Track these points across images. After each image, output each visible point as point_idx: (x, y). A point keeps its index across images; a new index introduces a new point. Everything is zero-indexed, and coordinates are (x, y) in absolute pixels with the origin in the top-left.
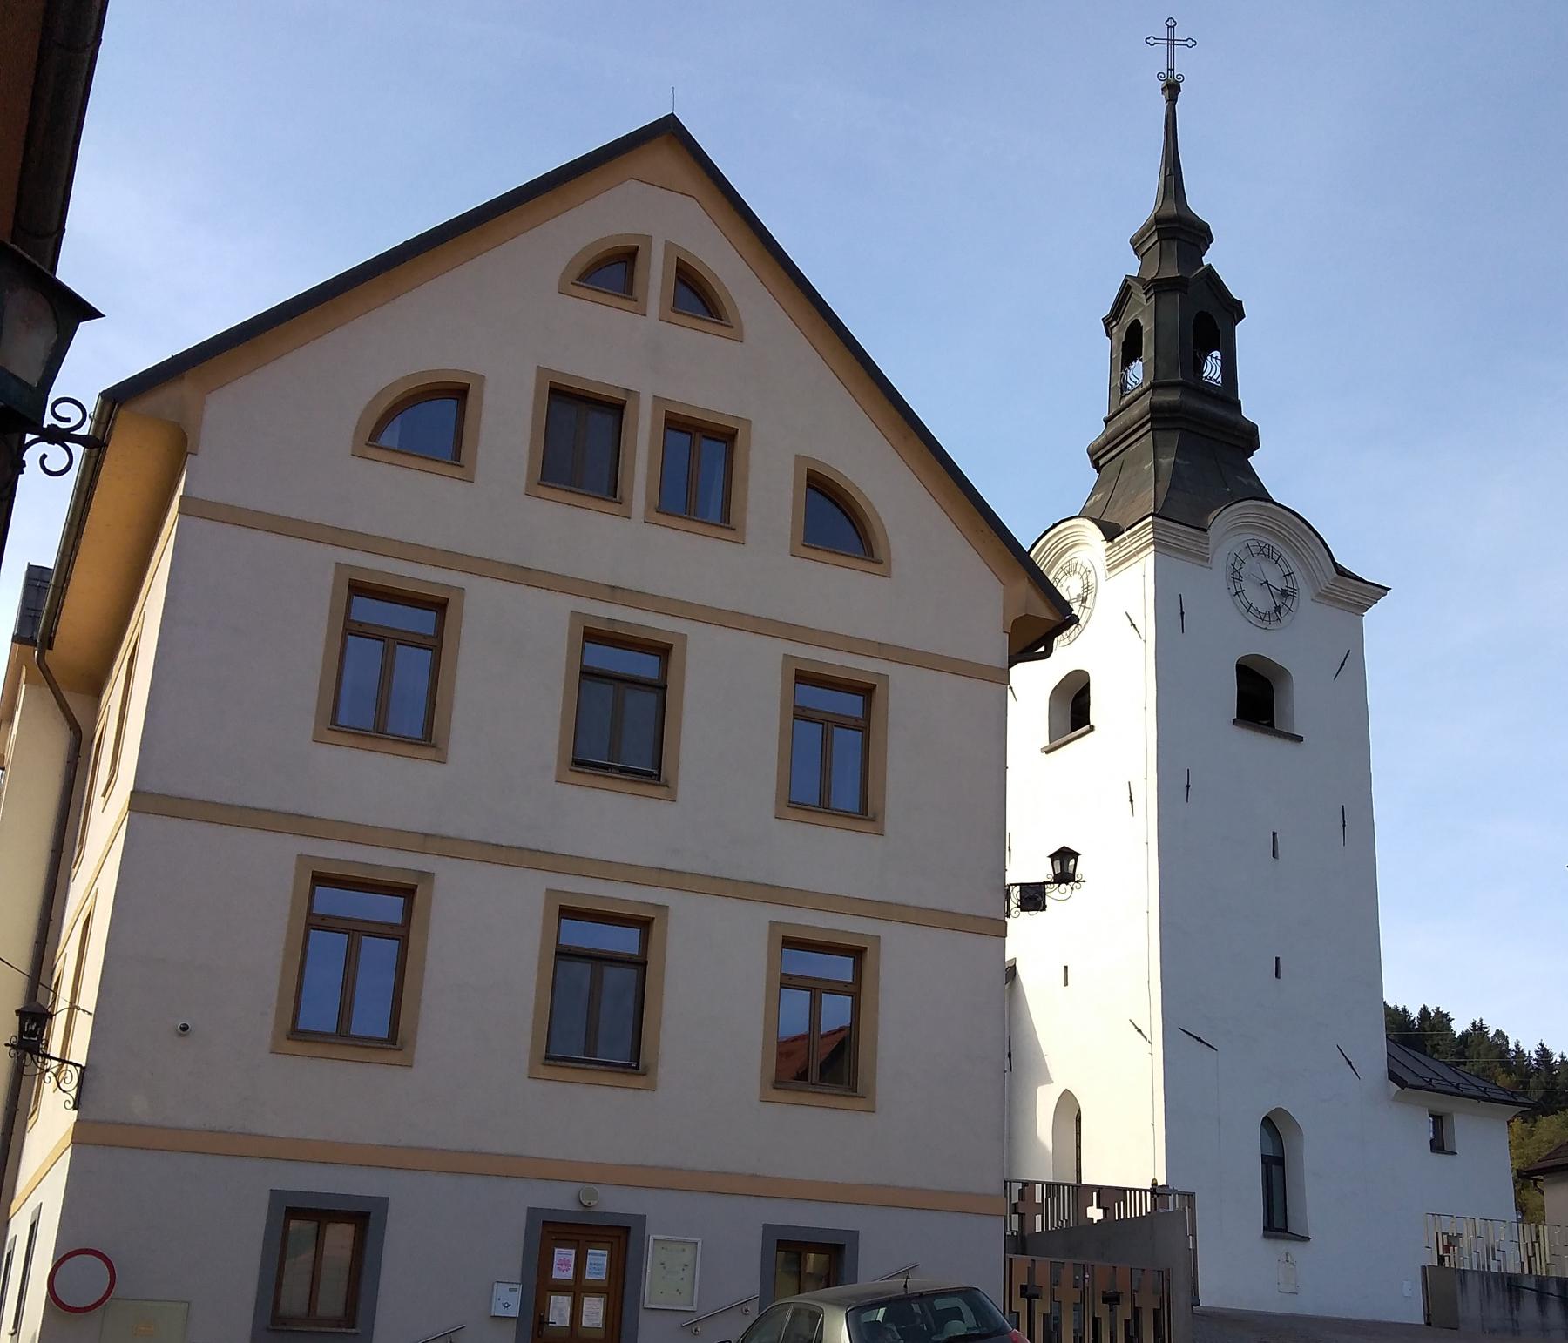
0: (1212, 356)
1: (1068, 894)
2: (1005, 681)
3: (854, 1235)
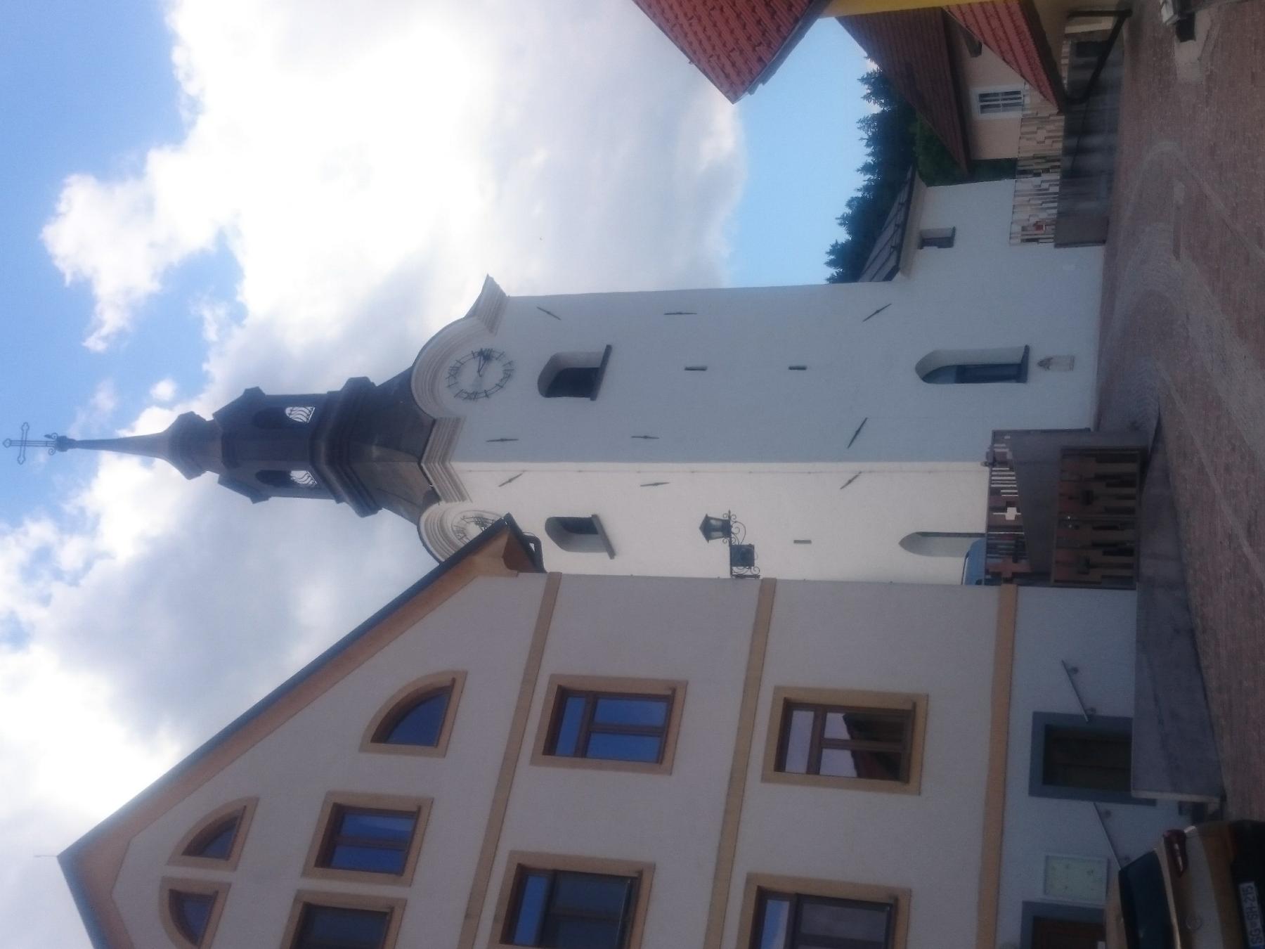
0: (290, 414)
1: (741, 527)
2: (551, 573)
3: (1037, 716)
